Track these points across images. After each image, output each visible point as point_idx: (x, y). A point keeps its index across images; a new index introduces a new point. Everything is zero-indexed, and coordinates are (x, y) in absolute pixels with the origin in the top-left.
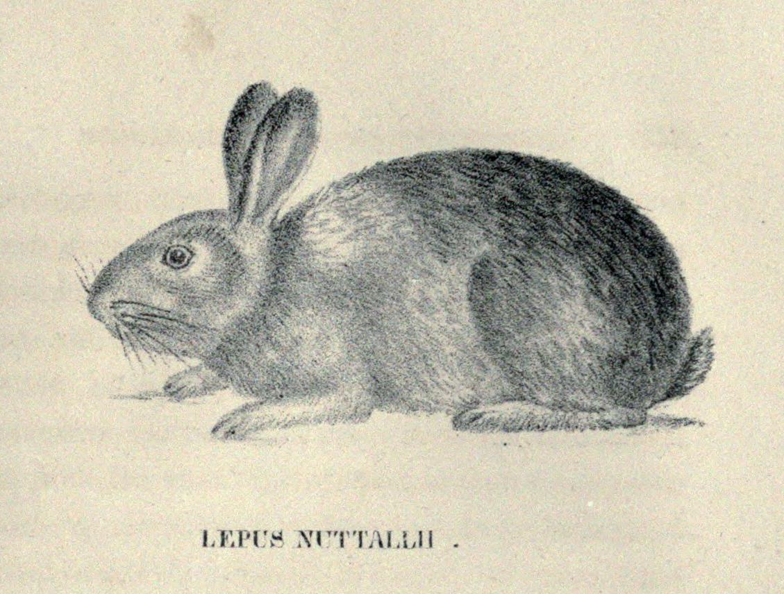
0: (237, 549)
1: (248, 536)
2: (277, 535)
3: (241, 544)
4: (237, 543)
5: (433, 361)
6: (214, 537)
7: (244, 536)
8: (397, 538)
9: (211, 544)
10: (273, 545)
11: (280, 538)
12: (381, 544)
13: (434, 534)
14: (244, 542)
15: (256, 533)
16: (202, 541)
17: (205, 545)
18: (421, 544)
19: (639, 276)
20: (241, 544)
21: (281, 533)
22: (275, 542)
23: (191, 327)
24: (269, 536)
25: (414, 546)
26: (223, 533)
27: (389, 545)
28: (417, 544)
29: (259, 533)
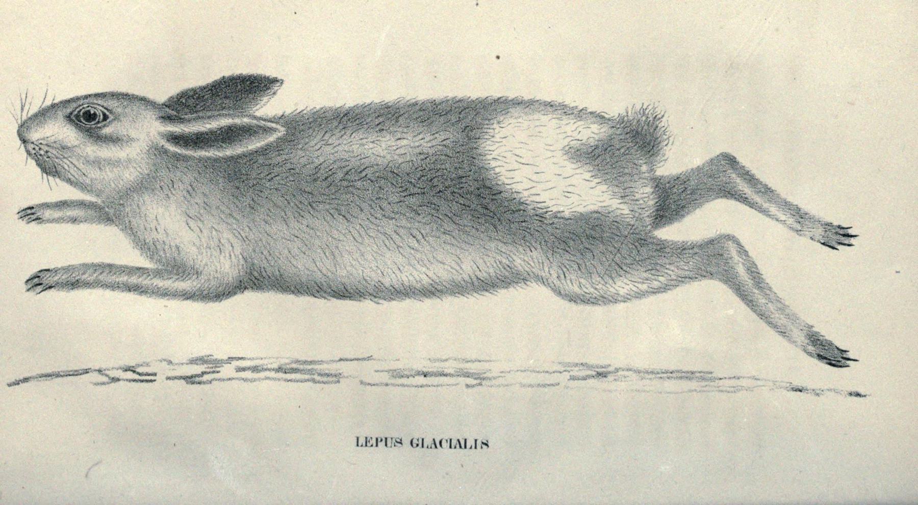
0: (374, 448)
1: (381, 440)
2: (399, 440)
3: (377, 446)
4: (375, 444)
5: (721, 273)
6: (362, 441)
7: (379, 440)
8: (470, 443)
9: (470, 447)
10: (482, 448)
11: (401, 443)
12: (460, 447)
13: (424, 440)
14: (379, 444)
15: (386, 439)
16: (356, 443)
17: (358, 445)
18: (476, 448)
19: (565, 284)
20: (377, 446)
21: (401, 440)
22: (396, 444)
23: (550, 274)
24: (394, 440)
25: (471, 448)
26: (366, 438)
27: (465, 447)
28: (473, 447)
29: (388, 439)
